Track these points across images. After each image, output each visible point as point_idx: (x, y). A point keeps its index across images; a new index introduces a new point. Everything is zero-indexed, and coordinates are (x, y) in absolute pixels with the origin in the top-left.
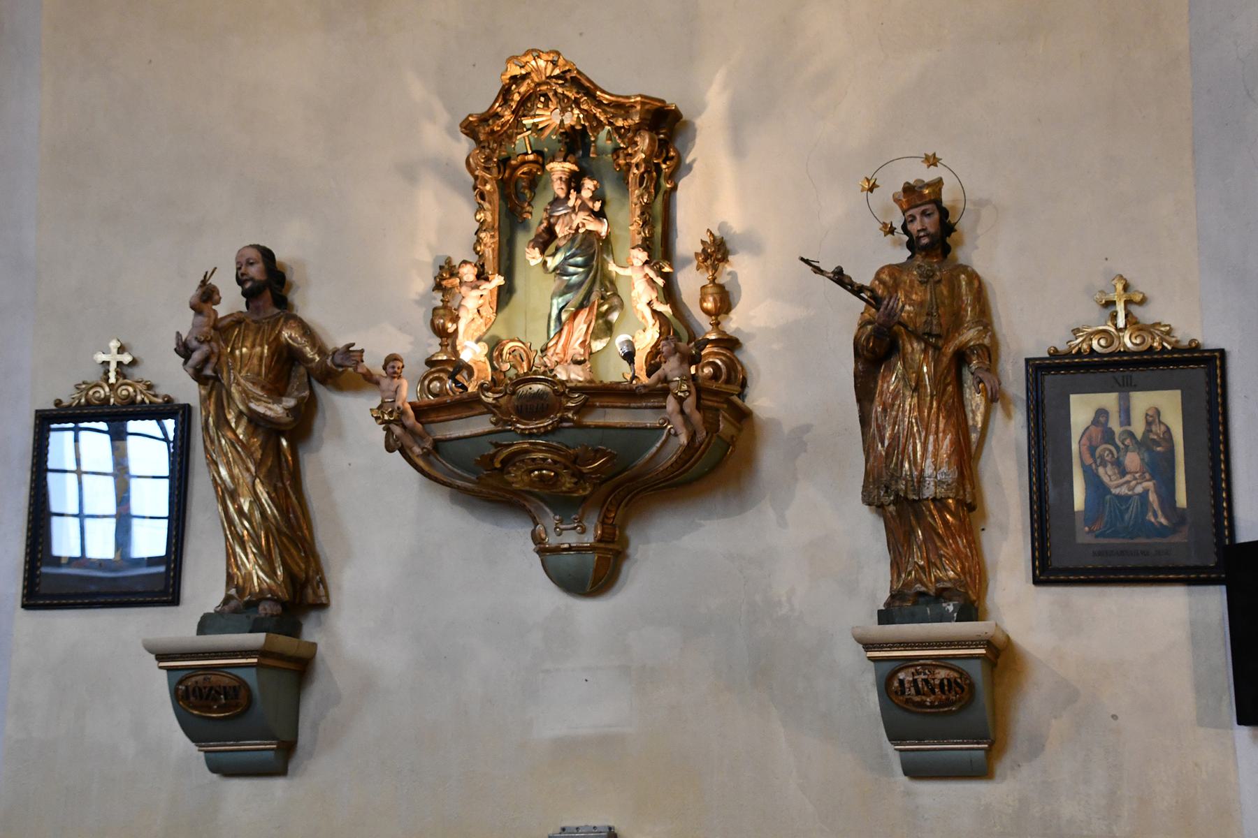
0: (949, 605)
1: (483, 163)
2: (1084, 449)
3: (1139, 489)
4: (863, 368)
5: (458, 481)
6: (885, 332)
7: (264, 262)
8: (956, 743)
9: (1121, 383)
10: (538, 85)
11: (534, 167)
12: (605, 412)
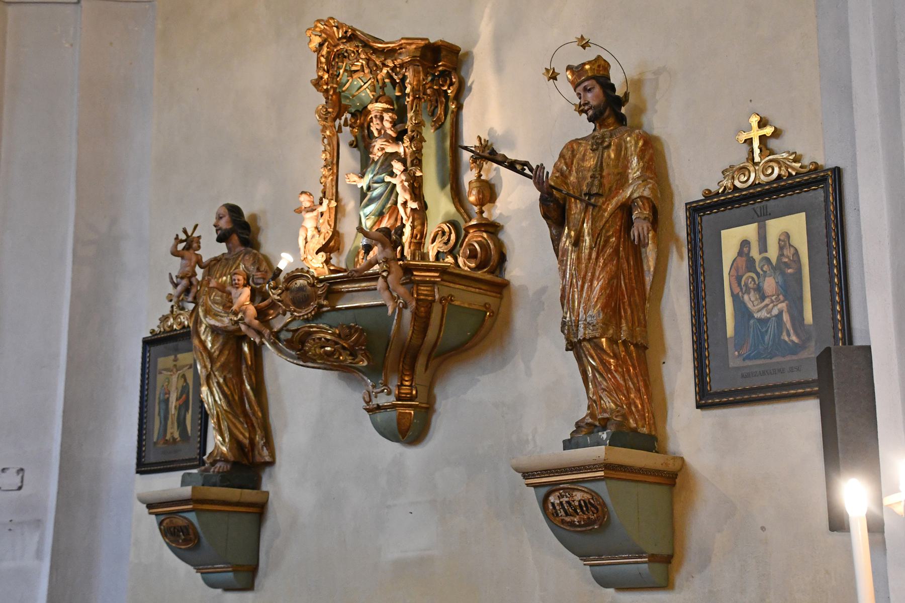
0: (603, 434)
2: (733, 279)
3: (775, 312)
4: (556, 232)
6: (547, 198)
7: (231, 216)
8: (625, 558)
9: (760, 215)
12: (352, 295)
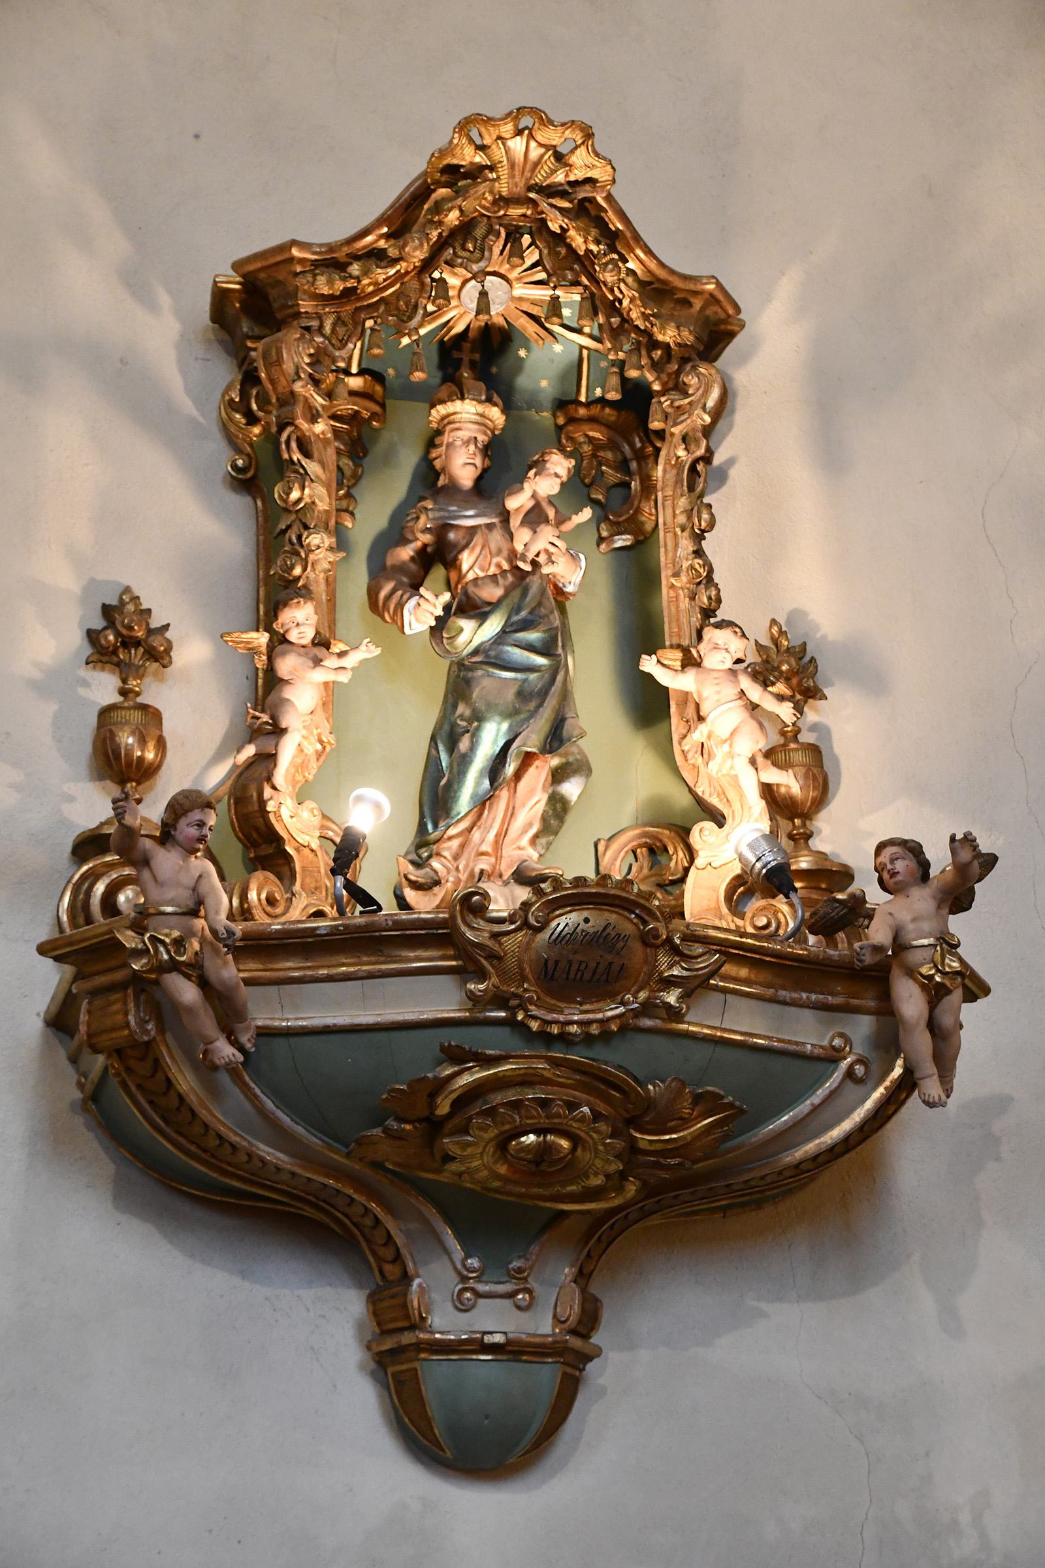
1: (308, 364)
5: (262, 1146)
10: (503, 201)
11: (365, 409)
